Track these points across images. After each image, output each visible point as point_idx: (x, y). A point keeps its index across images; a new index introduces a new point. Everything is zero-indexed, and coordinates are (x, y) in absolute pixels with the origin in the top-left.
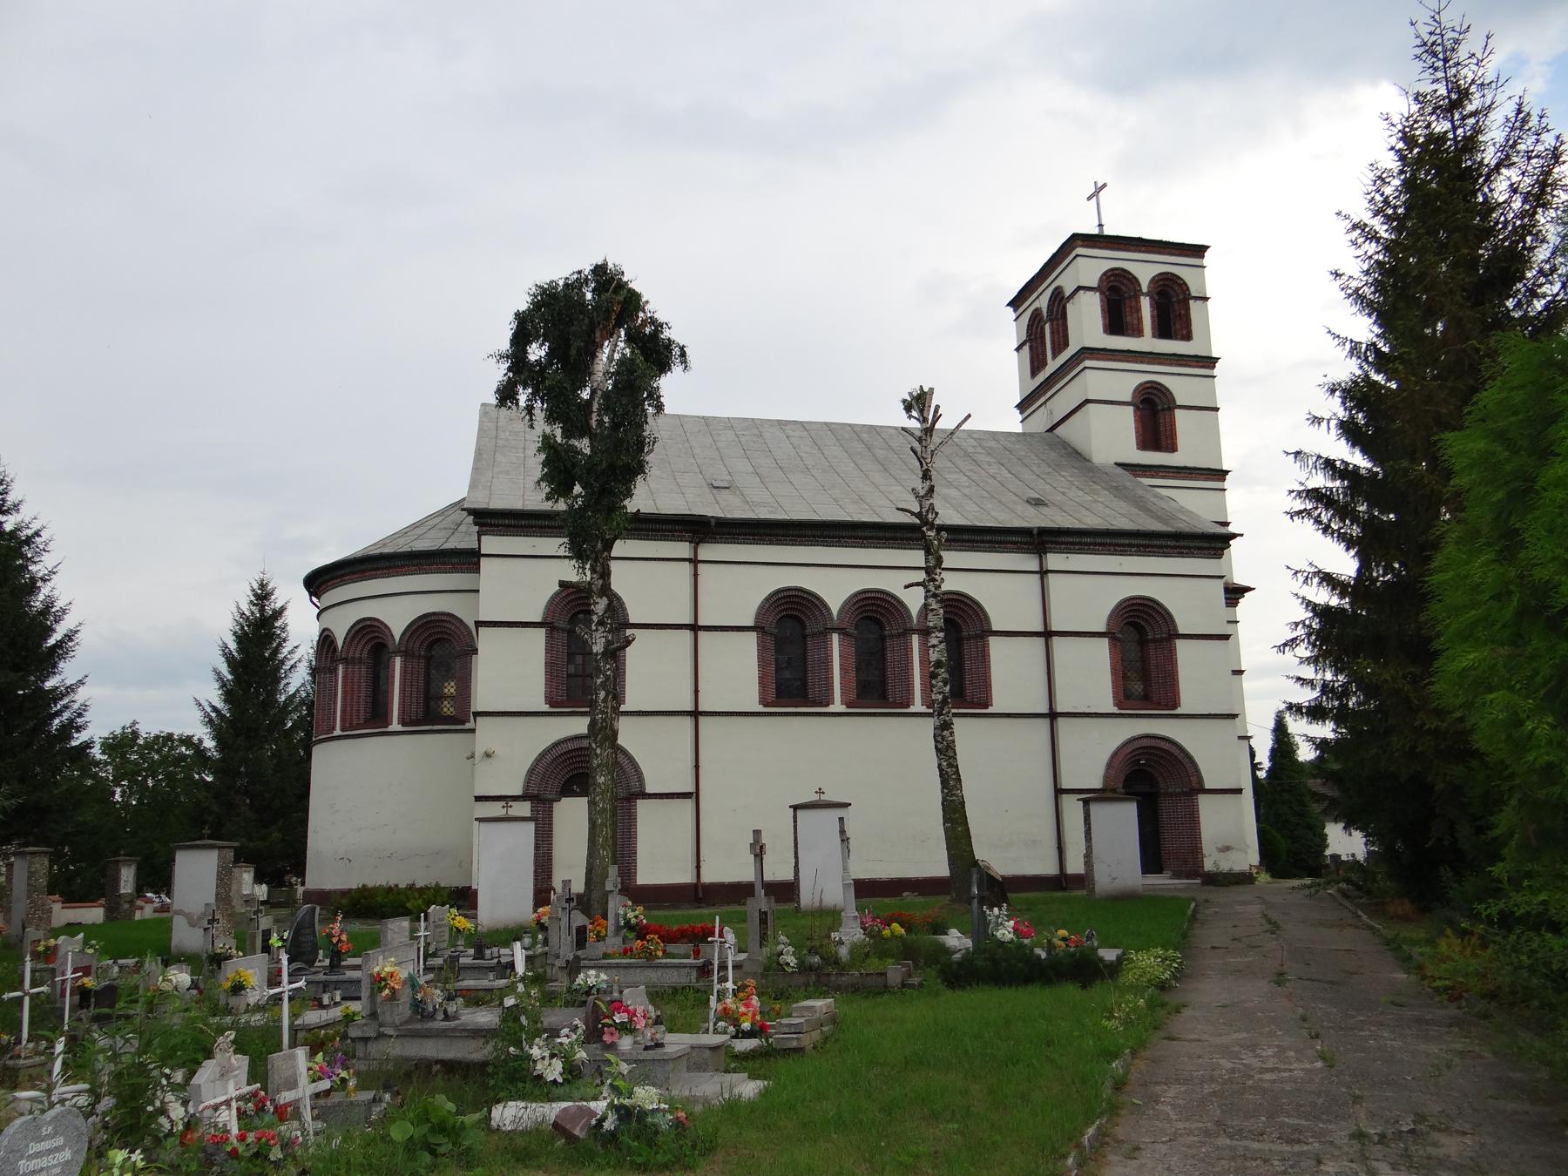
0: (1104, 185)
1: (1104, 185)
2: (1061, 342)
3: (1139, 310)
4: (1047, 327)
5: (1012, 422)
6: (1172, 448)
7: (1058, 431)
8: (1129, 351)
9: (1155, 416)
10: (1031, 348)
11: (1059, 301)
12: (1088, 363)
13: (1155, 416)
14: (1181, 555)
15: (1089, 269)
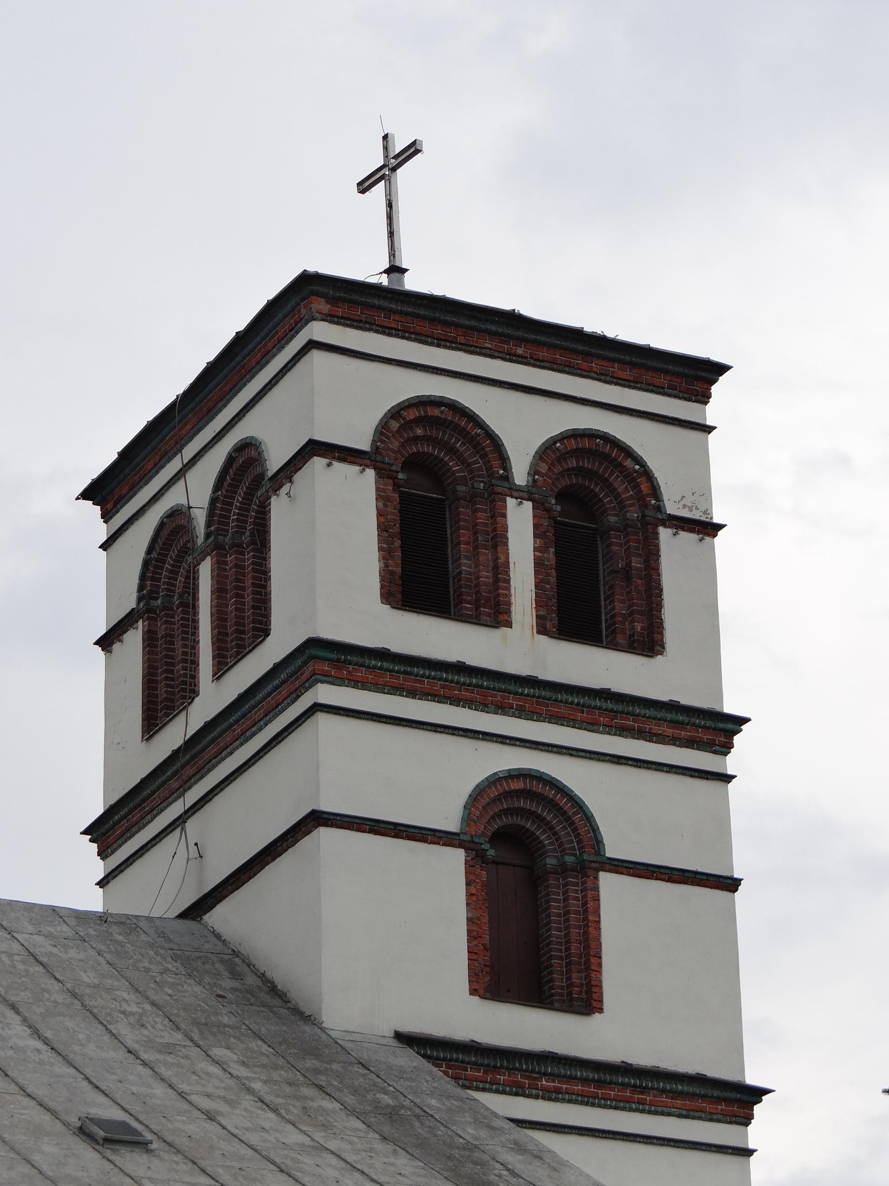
0: (413, 150)
1: (413, 150)
2: (246, 621)
3: (498, 539)
4: (205, 571)
5: (73, 879)
6: (585, 999)
7: (218, 917)
8: (460, 668)
9: (534, 892)
10: (149, 640)
11: (249, 486)
12: (325, 693)
13: (534, 892)
14: (288, 342)
15: (347, 392)
